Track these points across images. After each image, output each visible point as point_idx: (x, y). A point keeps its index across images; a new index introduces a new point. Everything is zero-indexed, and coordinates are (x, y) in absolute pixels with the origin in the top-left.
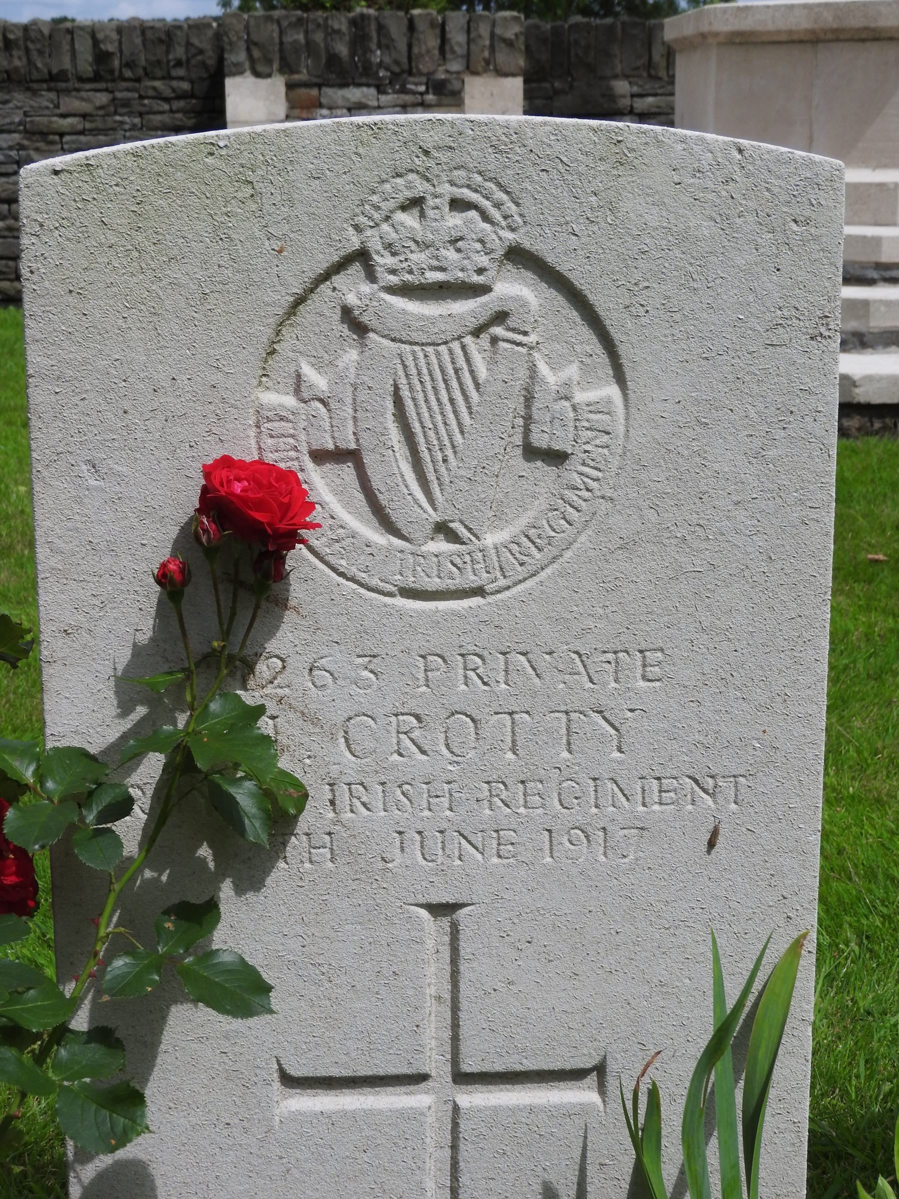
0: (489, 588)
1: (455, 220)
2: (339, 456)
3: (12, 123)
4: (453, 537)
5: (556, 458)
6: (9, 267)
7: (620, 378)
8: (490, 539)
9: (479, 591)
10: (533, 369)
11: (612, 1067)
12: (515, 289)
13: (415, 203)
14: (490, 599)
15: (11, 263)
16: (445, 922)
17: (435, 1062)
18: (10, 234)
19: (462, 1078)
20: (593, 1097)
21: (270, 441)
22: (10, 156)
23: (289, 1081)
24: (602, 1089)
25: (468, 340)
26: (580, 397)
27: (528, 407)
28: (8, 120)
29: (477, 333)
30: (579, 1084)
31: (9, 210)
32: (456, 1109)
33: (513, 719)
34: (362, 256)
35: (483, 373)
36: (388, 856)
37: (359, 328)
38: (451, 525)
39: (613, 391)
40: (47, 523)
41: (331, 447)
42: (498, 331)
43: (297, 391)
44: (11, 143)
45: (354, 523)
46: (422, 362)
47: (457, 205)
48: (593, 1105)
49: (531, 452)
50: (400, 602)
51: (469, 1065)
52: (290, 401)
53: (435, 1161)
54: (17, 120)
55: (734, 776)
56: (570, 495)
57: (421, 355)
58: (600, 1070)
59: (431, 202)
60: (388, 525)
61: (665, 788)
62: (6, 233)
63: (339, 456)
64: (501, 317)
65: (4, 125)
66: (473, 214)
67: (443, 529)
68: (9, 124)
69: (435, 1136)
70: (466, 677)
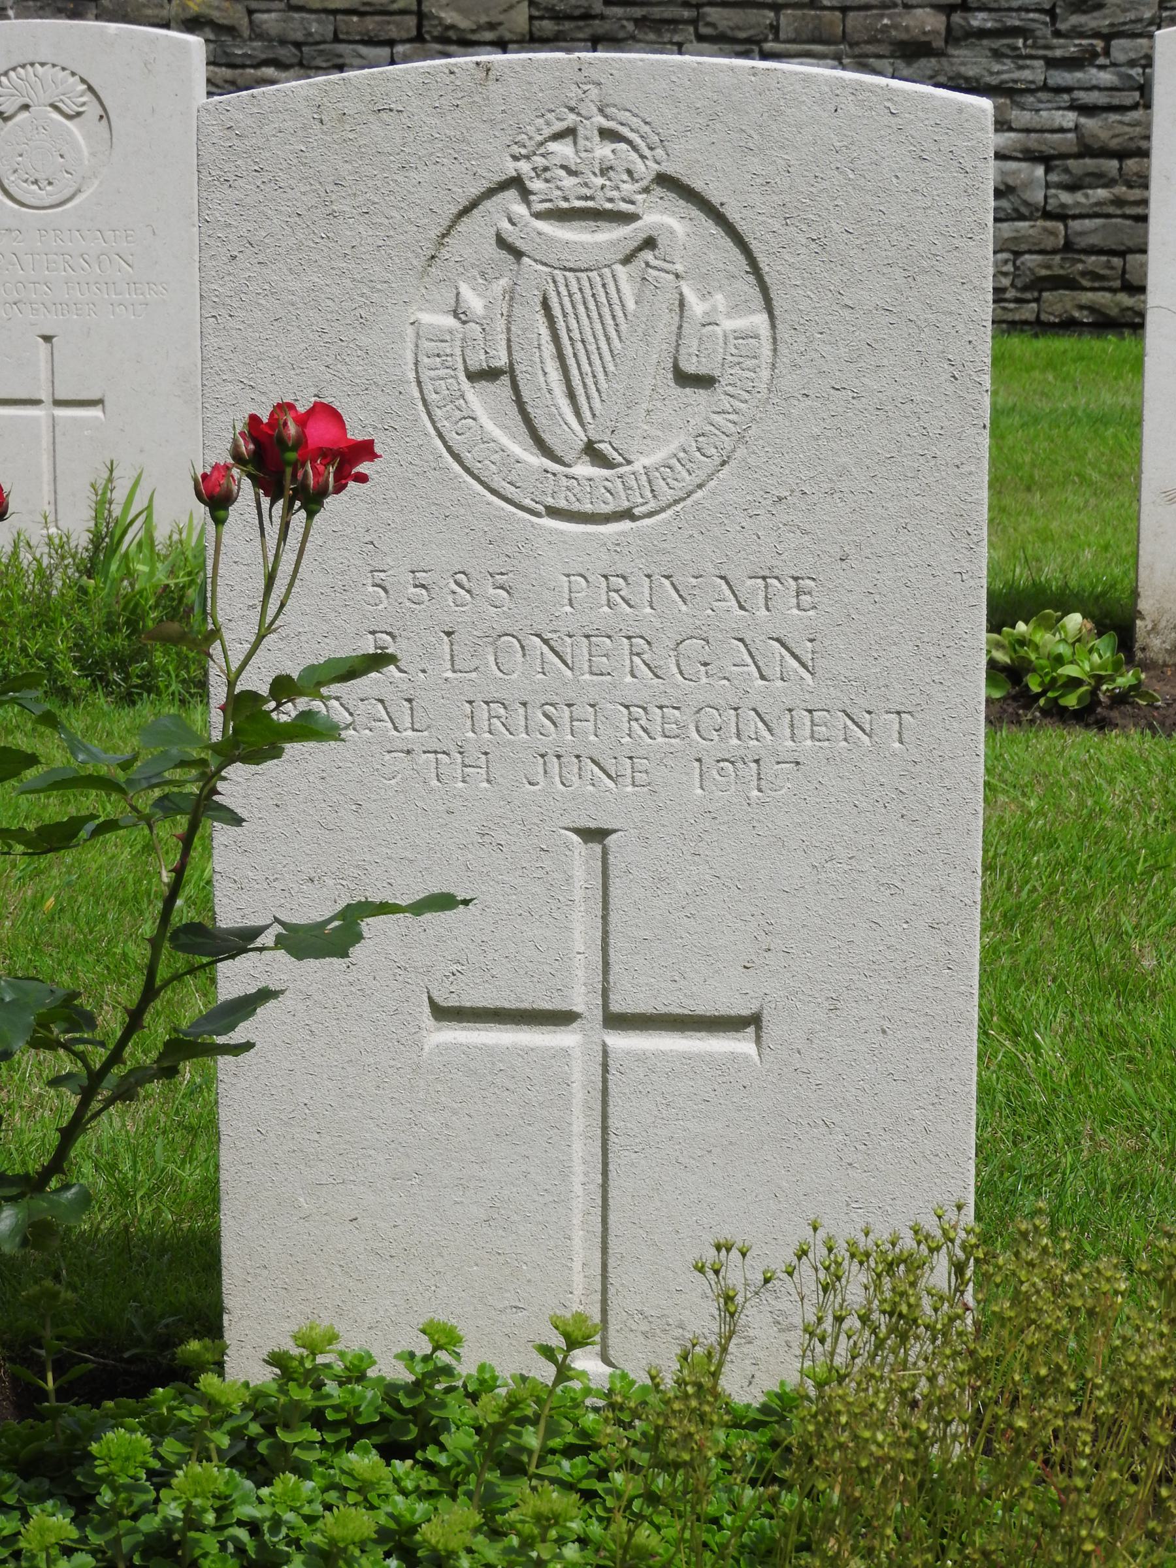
0: (636, 511)
1: (604, 150)
2: (490, 374)
3: (1140, 20)
5: (705, 382)
6: (1112, 268)
9: (627, 514)
11: (766, 1017)
13: (569, 133)
14: (638, 523)
15: (1116, 261)
16: (598, 848)
17: (581, 999)
18: (1119, 212)
19: (616, 1021)
21: (426, 360)
22: (1130, 77)
23: (444, 1013)
24: (758, 1040)
25: (619, 268)
28: (1132, 15)
29: (627, 260)
30: (739, 1035)
31: (1121, 169)
32: (604, 1045)
34: (516, 183)
35: (631, 305)
36: (534, 779)
39: (760, 320)
42: (648, 255)
44: (1133, 55)
46: (574, 288)
47: (607, 135)
48: (746, 1057)
49: (684, 379)
50: (548, 522)
51: (615, 1008)
52: (450, 321)
54: (1148, 15)
56: (717, 419)
59: (581, 132)
60: (544, 449)
61: (467, 761)
62: (1111, 210)
63: (490, 374)
64: (650, 243)
65: (1125, 23)
66: (623, 146)
67: (592, 452)
68: (1132, 22)
69: (581, 1078)
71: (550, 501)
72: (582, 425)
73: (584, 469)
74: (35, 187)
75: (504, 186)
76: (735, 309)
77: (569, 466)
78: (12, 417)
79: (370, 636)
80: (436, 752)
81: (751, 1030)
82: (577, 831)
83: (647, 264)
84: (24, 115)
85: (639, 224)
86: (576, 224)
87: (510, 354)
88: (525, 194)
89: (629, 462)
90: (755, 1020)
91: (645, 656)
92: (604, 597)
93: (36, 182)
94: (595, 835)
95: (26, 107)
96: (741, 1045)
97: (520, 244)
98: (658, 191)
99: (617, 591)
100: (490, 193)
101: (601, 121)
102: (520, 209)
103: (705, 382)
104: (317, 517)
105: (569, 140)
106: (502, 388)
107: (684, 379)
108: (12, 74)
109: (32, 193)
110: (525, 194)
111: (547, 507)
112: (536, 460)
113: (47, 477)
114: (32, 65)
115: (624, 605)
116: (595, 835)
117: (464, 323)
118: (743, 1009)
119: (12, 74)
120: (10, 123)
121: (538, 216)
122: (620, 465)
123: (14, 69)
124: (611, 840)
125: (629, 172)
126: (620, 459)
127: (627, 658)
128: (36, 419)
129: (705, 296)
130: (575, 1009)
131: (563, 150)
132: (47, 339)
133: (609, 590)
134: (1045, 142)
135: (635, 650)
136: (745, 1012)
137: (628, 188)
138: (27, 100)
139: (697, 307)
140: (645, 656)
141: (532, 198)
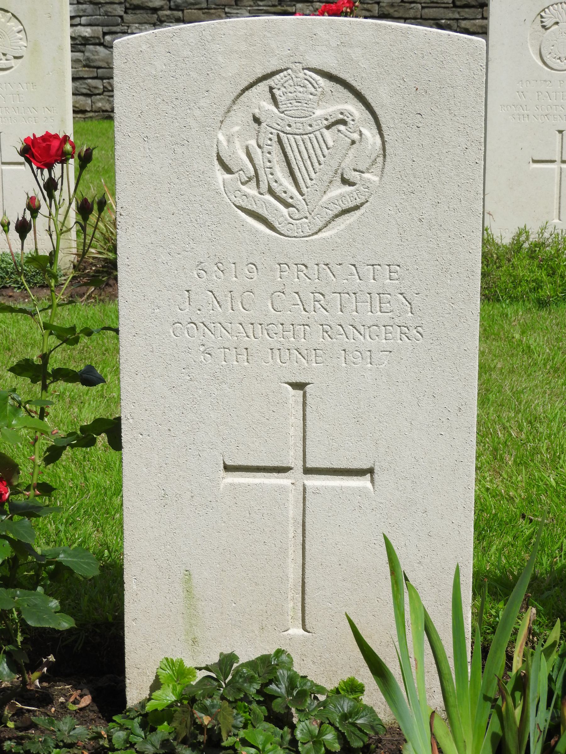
19: (308, 471)
20: (369, 485)
24: (372, 481)
29: (328, 128)
32: (304, 485)
51: (308, 465)
53: (293, 511)
70: (298, 275)
74: (559, 61)
78: (541, 169)
80: (224, 348)
81: (369, 475)
82: (291, 384)
84: (556, 27)
90: (371, 471)
91: (321, 302)
92: (296, 274)
93: (560, 58)
94: (299, 386)
95: (557, 23)
96: (364, 482)
104: (25, 241)
108: (551, 7)
109: (558, 63)
113: (556, 196)
114: (561, 3)
116: (299, 386)
118: (365, 466)
119: (551, 7)
120: (548, 31)
123: (552, 5)
124: (308, 388)
127: (313, 303)
128: (553, 169)
130: (289, 465)
132: (560, 132)
134: (475, 25)
135: (316, 299)
136: (365, 467)
138: (557, 20)
140: (321, 302)
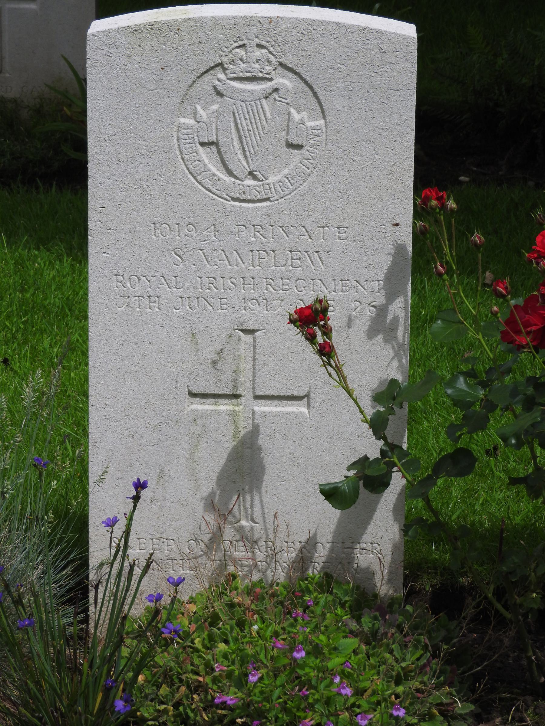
1: (259, 53)
2: (211, 144)
4: (255, 178)
5: (299, 147)
7: (324, 117)
8: (271, 180)
10: (289, 113)
12: (283, 81)
24: (309, 406)
25: (264, 101)
26: (309, 124)
27: (254, 353)
29: (266, 97)
33: (275, 254)
34: (221, 64)
35: (269, 116)
37: (220, 94)
38: (254, 173)
39: (322, 122)
40: (345, 319)
41: (207, 141)
43: (195, 118)
45: (214, 170)
47: (259, 46)
49: (291, 146)
50: (232, 203)
52: (192, 122)
55: (378, 281)
57: (244, 106)
58: (308, 396)
60: (230, 173)
64: (276, 90)
71: (233, 195)
72: (248, 163)
73: (250, 182)
75: (217, 66)
76: (315, 119)
77: (243, 181)
79: (340, 282)
83: (275, 99)
85: (273, 83)
86: (255, 83)
87: (217, 136)
88: (225, 70)
89: (266, 179)
96: (300, 408)
97: (223, 92)
98: (280, 68)
99: (258, 232)
100: (212, 68)
101: (257, 41)
102: (222, 76)
103: (299, 147)
105: (243, 48)
106: (214, 148)
107: (291, 146)
110: (225, 70)
111: (231, 197)
112: (228, 179)
115: (262, 238)
117: (199, 122)
121: (228, 79)
122: (263, 180)
125: (268, 61)
126: (264, 179)
129: (298, 112)
131: (241, 52)
133: (255, 231)
137: (268, 68)
139: (297, 116)
141: (227, 72)
